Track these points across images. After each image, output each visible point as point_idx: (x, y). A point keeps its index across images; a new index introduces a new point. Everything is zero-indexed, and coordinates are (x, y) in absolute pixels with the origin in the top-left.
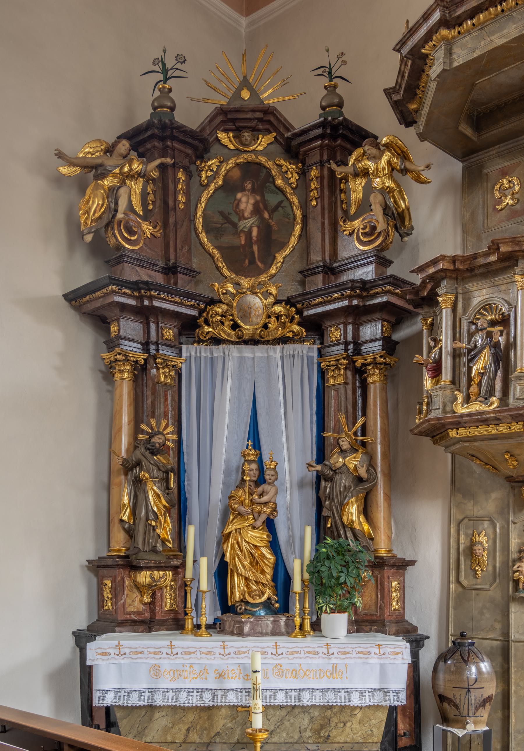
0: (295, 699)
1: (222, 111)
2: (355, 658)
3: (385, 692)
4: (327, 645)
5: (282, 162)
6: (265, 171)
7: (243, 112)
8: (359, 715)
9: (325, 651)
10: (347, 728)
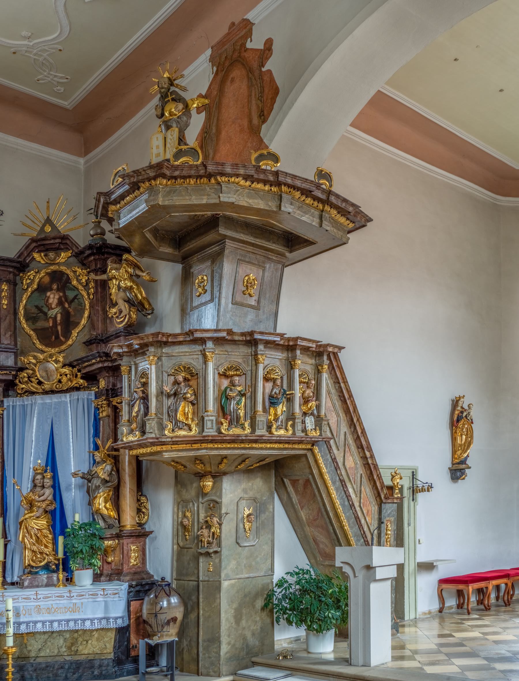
0: (49, 627)
1: (33, 240)
2: (88, 598)
3: (107, 619)
4: (70, 591)
5: (76, 268)
6: (66, 276)
7: (47, 240)
8: (96, 636)
9: (68, 595)
10: (89, 644)
